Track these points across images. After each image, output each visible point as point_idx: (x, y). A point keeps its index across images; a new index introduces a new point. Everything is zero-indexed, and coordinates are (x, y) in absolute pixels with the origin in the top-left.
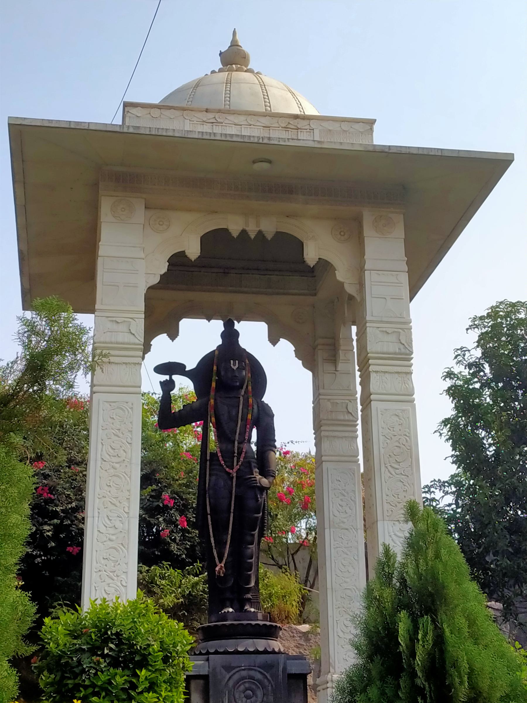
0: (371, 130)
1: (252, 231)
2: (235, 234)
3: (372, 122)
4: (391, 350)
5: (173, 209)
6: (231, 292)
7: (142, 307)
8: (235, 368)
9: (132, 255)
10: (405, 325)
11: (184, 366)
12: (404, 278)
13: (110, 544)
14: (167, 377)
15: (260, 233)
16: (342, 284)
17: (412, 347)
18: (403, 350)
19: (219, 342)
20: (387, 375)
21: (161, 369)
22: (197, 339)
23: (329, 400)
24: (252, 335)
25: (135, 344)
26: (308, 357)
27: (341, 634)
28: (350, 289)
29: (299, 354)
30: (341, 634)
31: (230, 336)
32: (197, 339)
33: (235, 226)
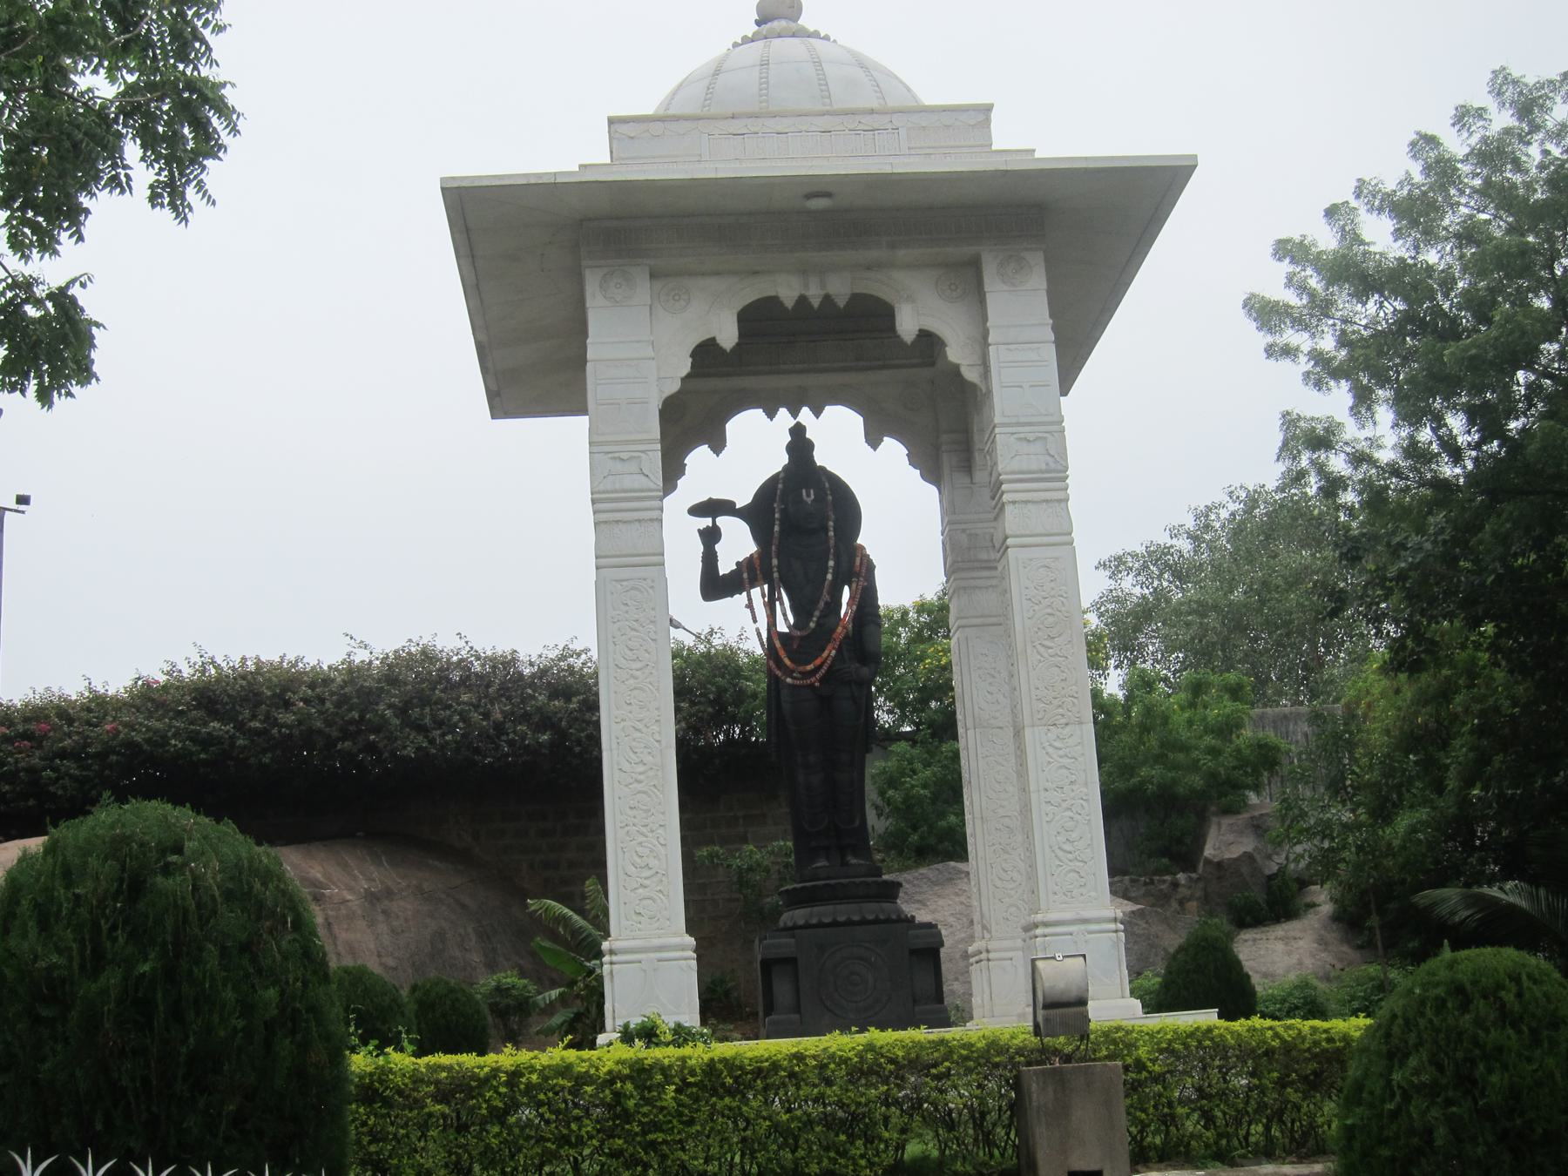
0: (988, 121)
1: (815, 295)
2: (789, 303)
3: (988, 109)
4: (1034, 467)
5: (691, 274)
6: (802, 372)
7: (655, 431)
8: (809, 500)
9: (642, 341)
10: (1056, 425)
11: (733, 504)
12: (1050, 353)
13: (639, 787)
14: (708, 522)
15: (827, 299)
16: (957, 367)
17: (1066, 460)
18: (1052, 466)
19: (784, 459)
20: (1030, 506)
21: (697, 510)
22: (752, 449)
23: (964, 531)
24: (838, 436)
25: (650, 490)
26: (929, 463)
27: (998, 883)
28: (970, 374)
29: (914, 460)
30: (998, 883)
31: (800, 445)
32: (752, 449)
33: (787, 290)
